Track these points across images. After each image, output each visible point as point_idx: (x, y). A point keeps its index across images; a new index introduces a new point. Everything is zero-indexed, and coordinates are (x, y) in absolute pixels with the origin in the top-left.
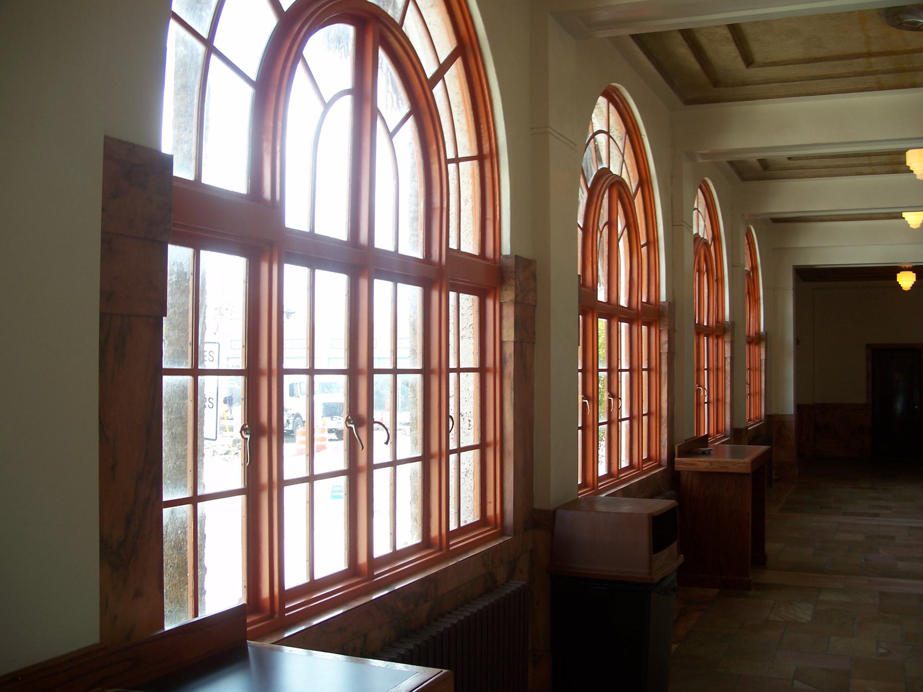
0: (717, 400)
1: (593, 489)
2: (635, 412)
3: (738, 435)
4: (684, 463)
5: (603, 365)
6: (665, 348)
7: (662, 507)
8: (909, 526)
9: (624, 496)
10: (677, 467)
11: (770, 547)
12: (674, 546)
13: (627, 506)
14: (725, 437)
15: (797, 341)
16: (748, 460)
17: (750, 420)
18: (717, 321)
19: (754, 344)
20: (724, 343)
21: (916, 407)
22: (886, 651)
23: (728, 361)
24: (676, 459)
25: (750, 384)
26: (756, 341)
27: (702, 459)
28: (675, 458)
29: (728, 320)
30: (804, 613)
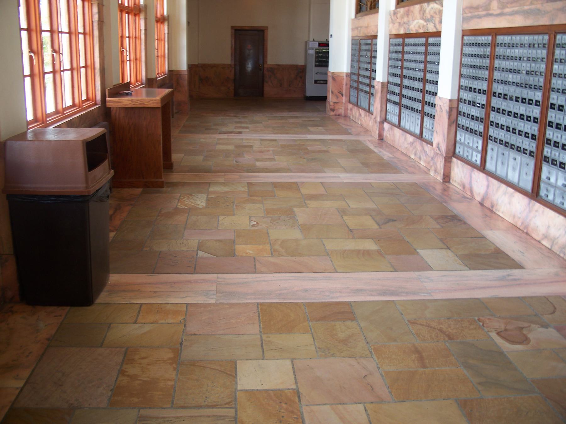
0: (136, 59)
1: (43, 123)
2: (75, 65)
3: (151, 83)
4: (112, 102)
5: (45, 25)
6: (96, 18)
7: (94, 134)
8: (260, 139)
9: (68, 127)
10: (108, 105)
11: (175, 157)
12: (106, 163)
13: (72, 135)
14: (142, 84)
15: (188, 23)
16: (158, 98)
17: (158, 74)
18: (135, 4)
19: (160, 22)
20: (140, 19)
21: (260, 66)
22: (256, 223)
23: (143, 32)
24: (107, 99)
25: (157, 49)
26: (162, 21)
27: (126, 98)
28: (106, 98)
29: (142, 3)
30: (200, 201)
